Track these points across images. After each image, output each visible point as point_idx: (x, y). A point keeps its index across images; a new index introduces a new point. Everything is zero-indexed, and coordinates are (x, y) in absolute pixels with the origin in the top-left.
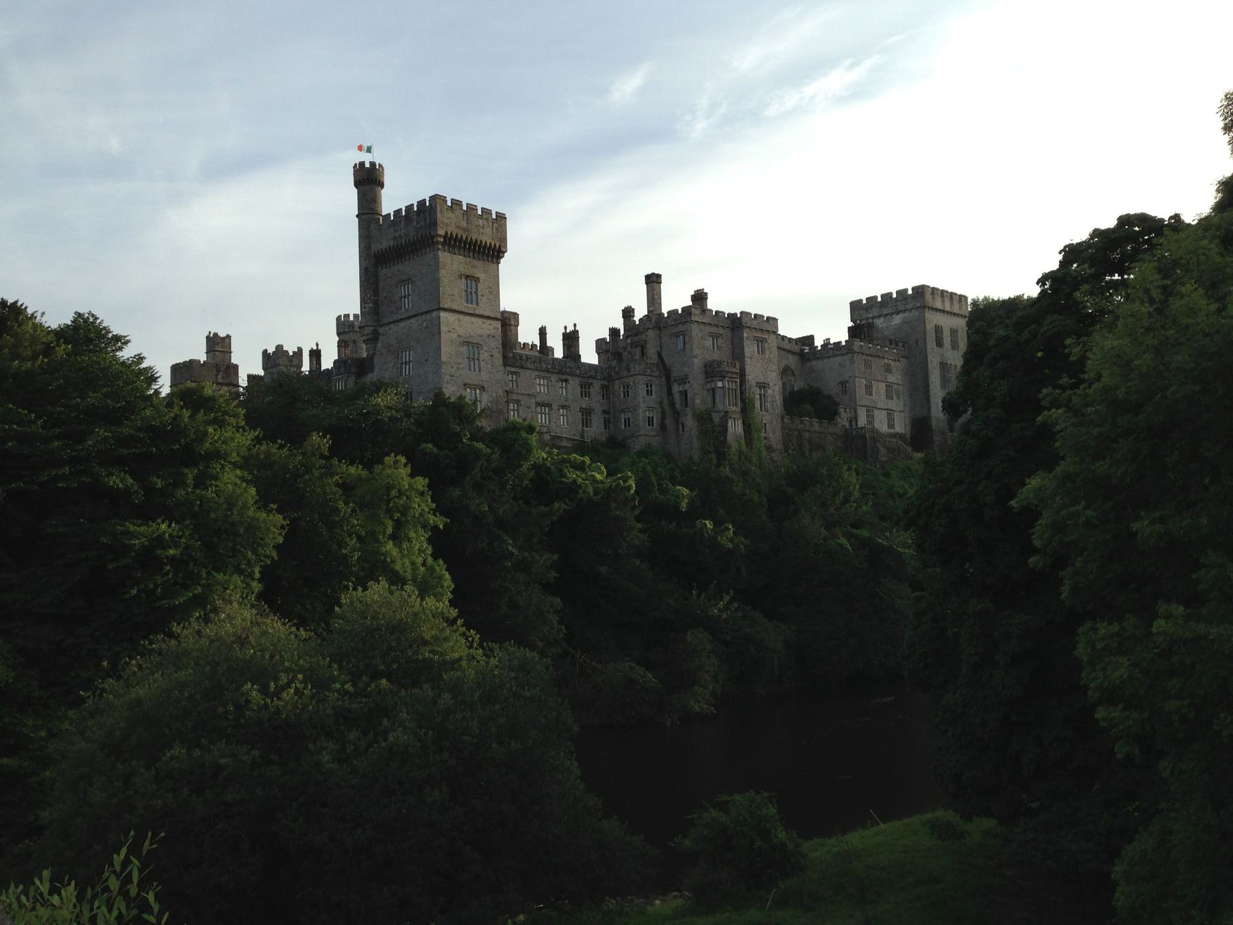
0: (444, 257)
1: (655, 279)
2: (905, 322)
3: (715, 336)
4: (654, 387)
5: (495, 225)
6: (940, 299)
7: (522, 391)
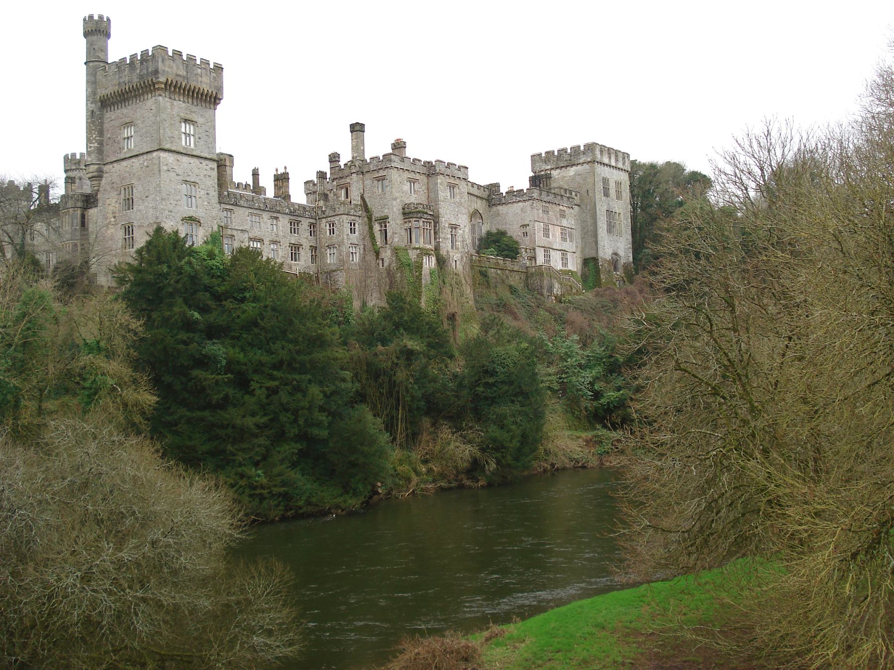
0: (163, 100)
1: (357, 128)
3: (412, 181)
7: (236, 228)
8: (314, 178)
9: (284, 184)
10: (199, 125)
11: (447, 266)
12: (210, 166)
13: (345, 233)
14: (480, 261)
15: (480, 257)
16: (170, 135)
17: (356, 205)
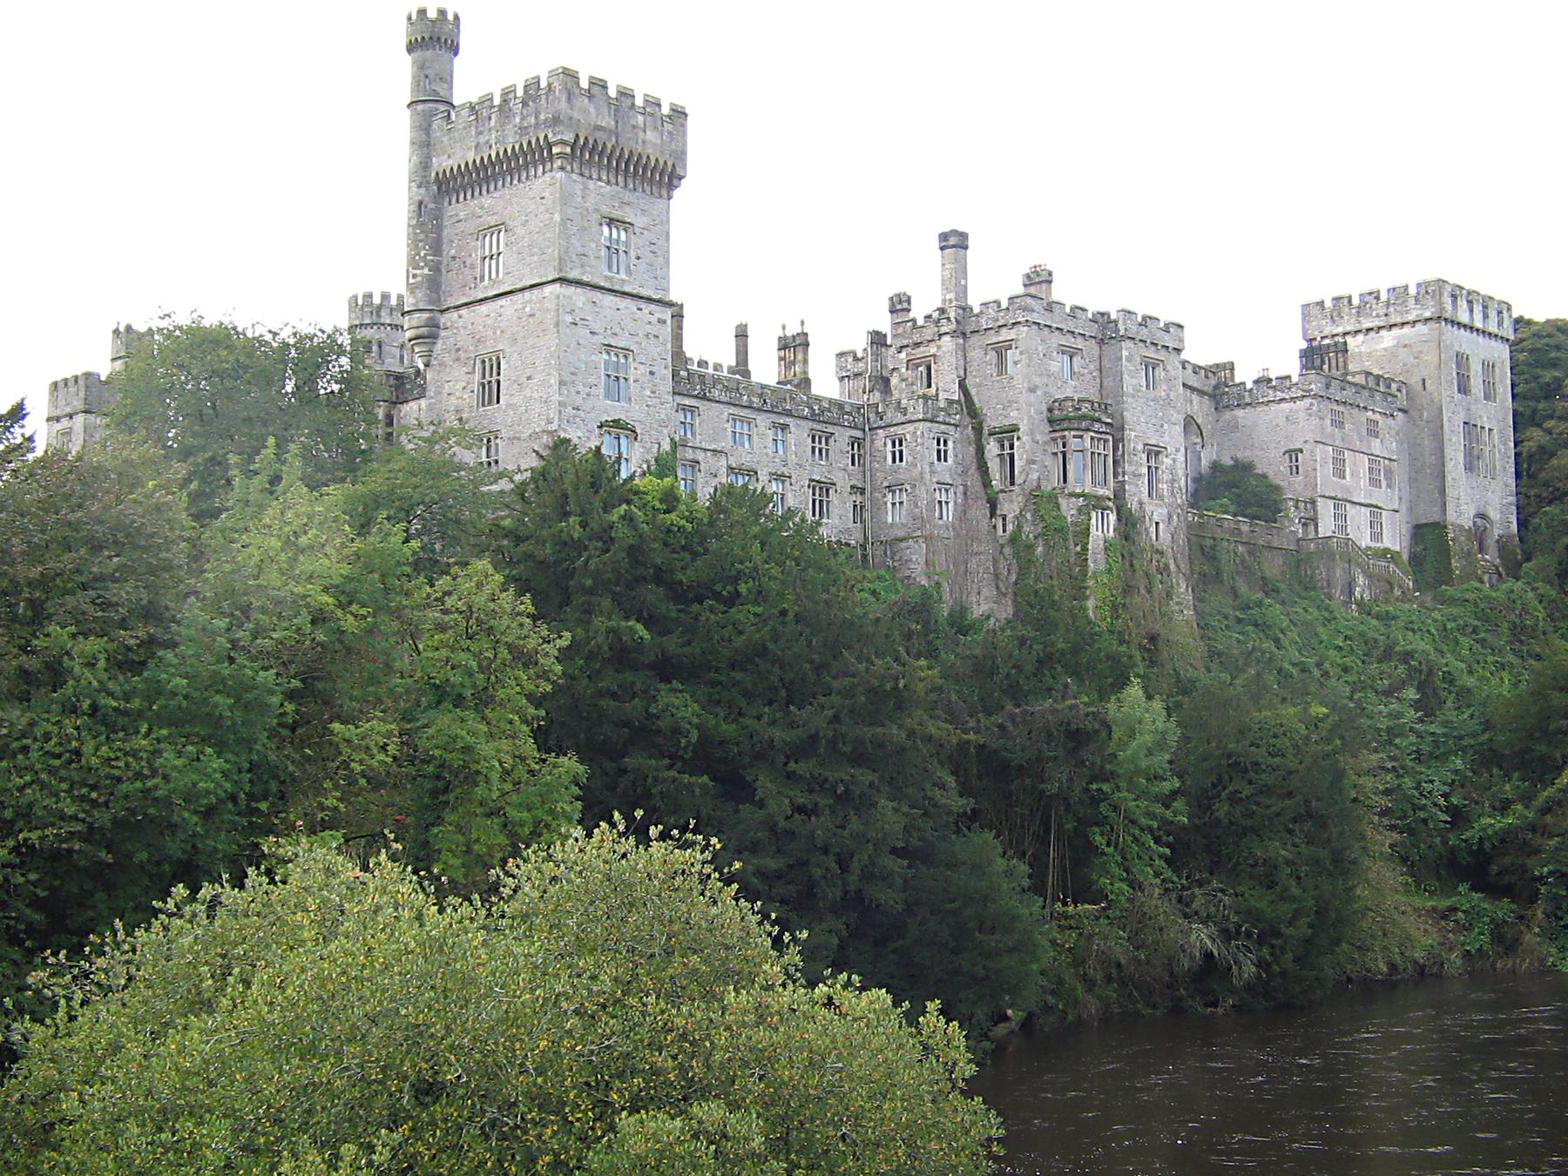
4: (950, 444)
7: (703, 445)
8: (860, 344)
10: (637, 230)
11: (1139, 534)
12: (658, 315)
14: (1201, 525)
15: (1201, 516)
16: (580, 250)
17: (950, 402)
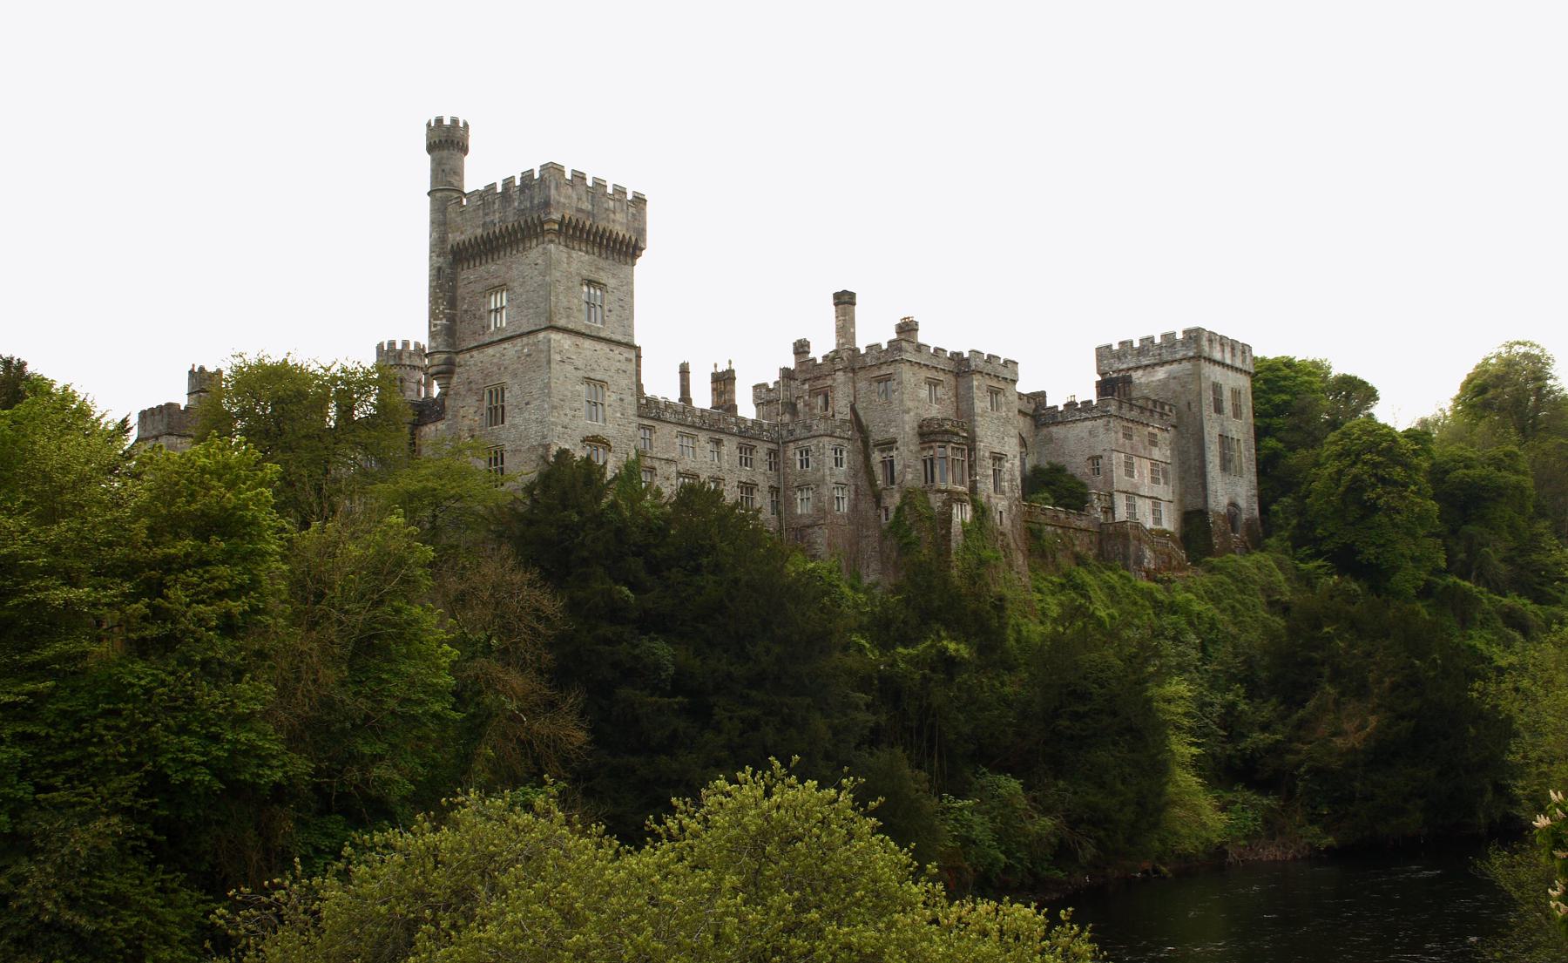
0: (556, 250)
1: (846, 298)
2: (1172, 377)
3: (933, 383)
4: (845, 454)
5: (631, 210)
6: (1218, 348)
7: (659, 455)
9: (728, 387)
10: (609, 289)
12: (626, 355)
13: (827, 466)
15: (1030, 507)
17: (844, 421)
